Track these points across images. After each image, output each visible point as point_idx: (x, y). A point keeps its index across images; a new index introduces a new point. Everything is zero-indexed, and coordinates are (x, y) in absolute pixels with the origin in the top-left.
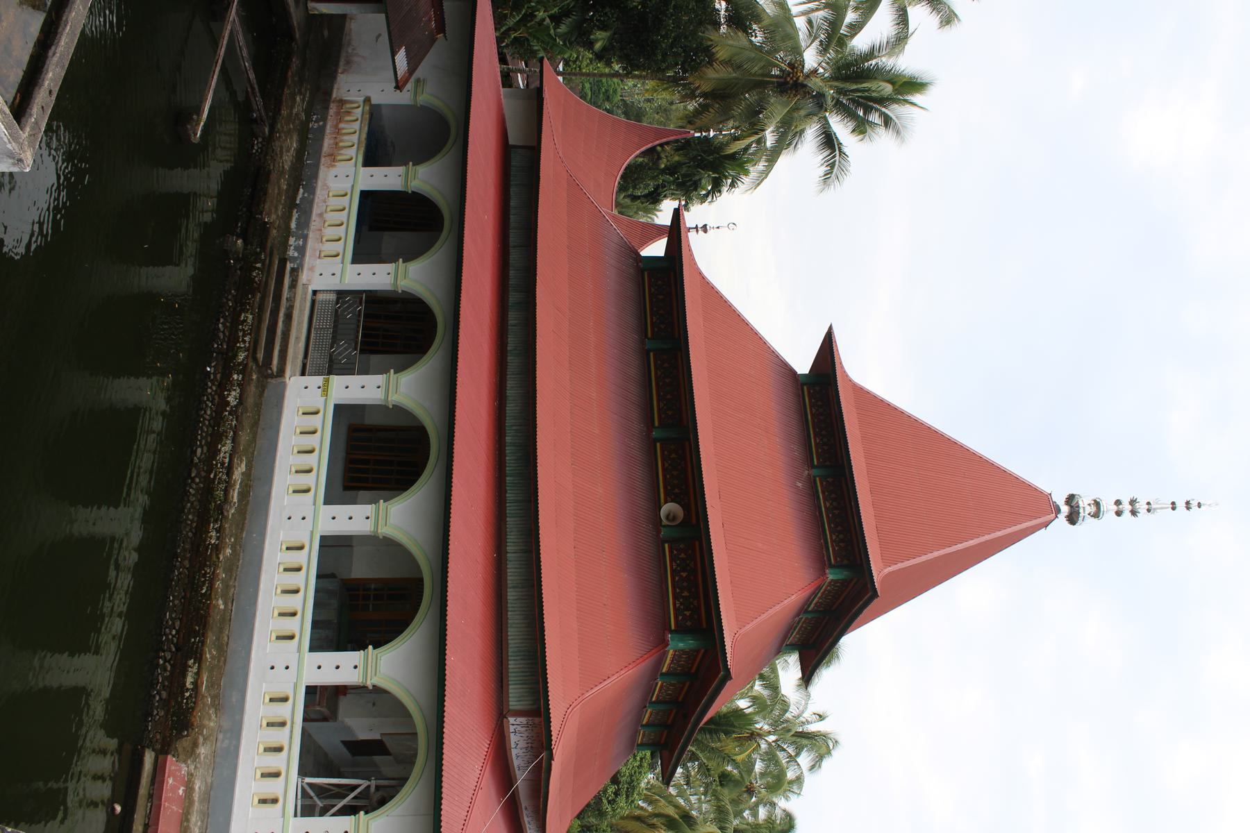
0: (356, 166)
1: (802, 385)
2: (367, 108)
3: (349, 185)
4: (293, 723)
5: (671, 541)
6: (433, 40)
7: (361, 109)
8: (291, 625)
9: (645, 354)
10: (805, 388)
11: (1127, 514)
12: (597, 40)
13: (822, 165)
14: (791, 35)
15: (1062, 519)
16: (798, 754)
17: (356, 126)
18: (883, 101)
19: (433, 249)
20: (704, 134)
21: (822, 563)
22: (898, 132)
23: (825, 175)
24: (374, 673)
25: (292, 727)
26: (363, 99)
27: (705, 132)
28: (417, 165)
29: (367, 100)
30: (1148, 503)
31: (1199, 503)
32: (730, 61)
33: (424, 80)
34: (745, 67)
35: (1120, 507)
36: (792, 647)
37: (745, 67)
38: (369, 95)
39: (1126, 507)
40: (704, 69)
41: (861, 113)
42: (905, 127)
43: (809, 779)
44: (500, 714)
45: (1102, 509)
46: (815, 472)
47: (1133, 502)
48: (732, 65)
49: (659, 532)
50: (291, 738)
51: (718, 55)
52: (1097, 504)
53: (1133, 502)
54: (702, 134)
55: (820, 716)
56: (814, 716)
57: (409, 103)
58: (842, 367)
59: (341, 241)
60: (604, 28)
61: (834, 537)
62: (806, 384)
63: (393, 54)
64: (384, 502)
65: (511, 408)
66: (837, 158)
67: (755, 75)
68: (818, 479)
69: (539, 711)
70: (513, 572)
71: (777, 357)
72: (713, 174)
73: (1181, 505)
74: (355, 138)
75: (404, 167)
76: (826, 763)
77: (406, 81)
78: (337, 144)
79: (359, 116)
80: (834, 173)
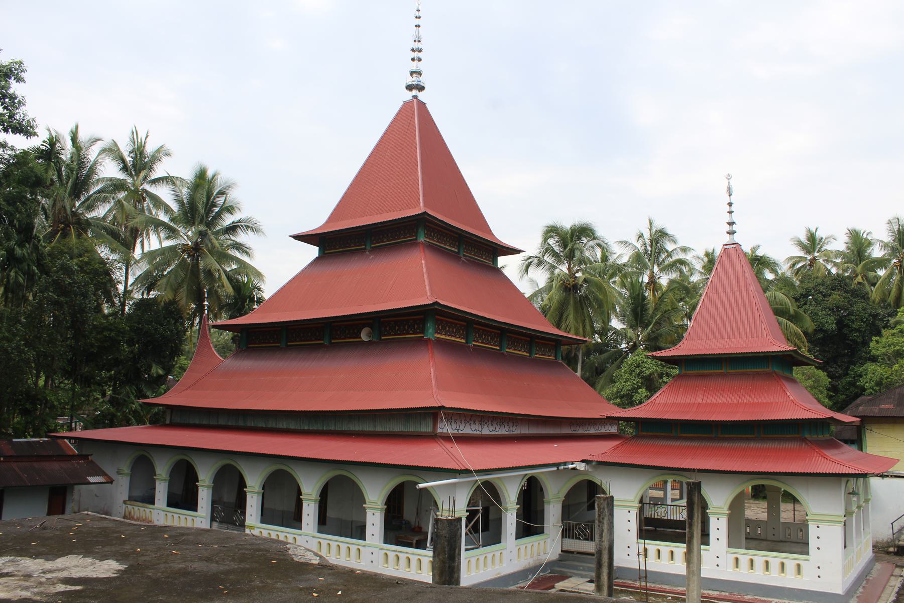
0: (154, 509)
1: (324, 254)
2: (128, 502)
3: (162, 512)
4: (396, 551)
5: (381, 335)
6: (92, 462)
7: (129, 506)
8: (354, 549)
9: (289, 348)
10: (326, 252)
11: (420, 55)
12: (157, 372)
13: (247, 233)
14: (172, 249)
15: (422, 96)
16: (667, 251)
17: (136, 508)
18: (209, 194)
19: (295, 477)
20: (206, 308)
21: (414, 244)
22: (229, 187)
23: (253, 231)
24: (376, 504)
25: (398, 551)
26: (124, 505)
27: (205, 307)
28: (155, 472)
29: (125, 502)
30: (415, 41)
31: (417, 10)
32: (175, 291)
33: (118, 469)
34: (180, 281)
35: (415, 58)
36: (495, 261)
37: (180, 281)
38: (122, 501)
39: (415, 55)
40: (180, 306)
41: (216, 209)
42: (226, 183)
43: (681, 243)
44: (433, 437)
45: (415, 70)
46: (368, 248)
47: (413, 50)
48: (177, 289)
49: (375, 342)
50: (403, 552)
51: (171, 298)
52: (412, 73)
53: (413, 50)
54: (206, 309)
55: (640, 237)
56: (639, 241)
57: (129, 478)
58: (315, 230)
59: (340, 545)
60: (150, 367)
61: (402, 237)
62: (324, 252)
63: (90, 483)
64: (302, 495)
65: (292, 426)
66: (243, 224)
67: (186, 275)
68: (372, 246)
69: (433, 413)
70: (368, 427)
71: (306, 268)
72: (246, 302)
73: (417, 22)
74: (142, 509)
75: (199, 487)
76: (670, 232)
77: (109, 477)
78: (143, 520)
79: (132, 507)
80: (252, 226)
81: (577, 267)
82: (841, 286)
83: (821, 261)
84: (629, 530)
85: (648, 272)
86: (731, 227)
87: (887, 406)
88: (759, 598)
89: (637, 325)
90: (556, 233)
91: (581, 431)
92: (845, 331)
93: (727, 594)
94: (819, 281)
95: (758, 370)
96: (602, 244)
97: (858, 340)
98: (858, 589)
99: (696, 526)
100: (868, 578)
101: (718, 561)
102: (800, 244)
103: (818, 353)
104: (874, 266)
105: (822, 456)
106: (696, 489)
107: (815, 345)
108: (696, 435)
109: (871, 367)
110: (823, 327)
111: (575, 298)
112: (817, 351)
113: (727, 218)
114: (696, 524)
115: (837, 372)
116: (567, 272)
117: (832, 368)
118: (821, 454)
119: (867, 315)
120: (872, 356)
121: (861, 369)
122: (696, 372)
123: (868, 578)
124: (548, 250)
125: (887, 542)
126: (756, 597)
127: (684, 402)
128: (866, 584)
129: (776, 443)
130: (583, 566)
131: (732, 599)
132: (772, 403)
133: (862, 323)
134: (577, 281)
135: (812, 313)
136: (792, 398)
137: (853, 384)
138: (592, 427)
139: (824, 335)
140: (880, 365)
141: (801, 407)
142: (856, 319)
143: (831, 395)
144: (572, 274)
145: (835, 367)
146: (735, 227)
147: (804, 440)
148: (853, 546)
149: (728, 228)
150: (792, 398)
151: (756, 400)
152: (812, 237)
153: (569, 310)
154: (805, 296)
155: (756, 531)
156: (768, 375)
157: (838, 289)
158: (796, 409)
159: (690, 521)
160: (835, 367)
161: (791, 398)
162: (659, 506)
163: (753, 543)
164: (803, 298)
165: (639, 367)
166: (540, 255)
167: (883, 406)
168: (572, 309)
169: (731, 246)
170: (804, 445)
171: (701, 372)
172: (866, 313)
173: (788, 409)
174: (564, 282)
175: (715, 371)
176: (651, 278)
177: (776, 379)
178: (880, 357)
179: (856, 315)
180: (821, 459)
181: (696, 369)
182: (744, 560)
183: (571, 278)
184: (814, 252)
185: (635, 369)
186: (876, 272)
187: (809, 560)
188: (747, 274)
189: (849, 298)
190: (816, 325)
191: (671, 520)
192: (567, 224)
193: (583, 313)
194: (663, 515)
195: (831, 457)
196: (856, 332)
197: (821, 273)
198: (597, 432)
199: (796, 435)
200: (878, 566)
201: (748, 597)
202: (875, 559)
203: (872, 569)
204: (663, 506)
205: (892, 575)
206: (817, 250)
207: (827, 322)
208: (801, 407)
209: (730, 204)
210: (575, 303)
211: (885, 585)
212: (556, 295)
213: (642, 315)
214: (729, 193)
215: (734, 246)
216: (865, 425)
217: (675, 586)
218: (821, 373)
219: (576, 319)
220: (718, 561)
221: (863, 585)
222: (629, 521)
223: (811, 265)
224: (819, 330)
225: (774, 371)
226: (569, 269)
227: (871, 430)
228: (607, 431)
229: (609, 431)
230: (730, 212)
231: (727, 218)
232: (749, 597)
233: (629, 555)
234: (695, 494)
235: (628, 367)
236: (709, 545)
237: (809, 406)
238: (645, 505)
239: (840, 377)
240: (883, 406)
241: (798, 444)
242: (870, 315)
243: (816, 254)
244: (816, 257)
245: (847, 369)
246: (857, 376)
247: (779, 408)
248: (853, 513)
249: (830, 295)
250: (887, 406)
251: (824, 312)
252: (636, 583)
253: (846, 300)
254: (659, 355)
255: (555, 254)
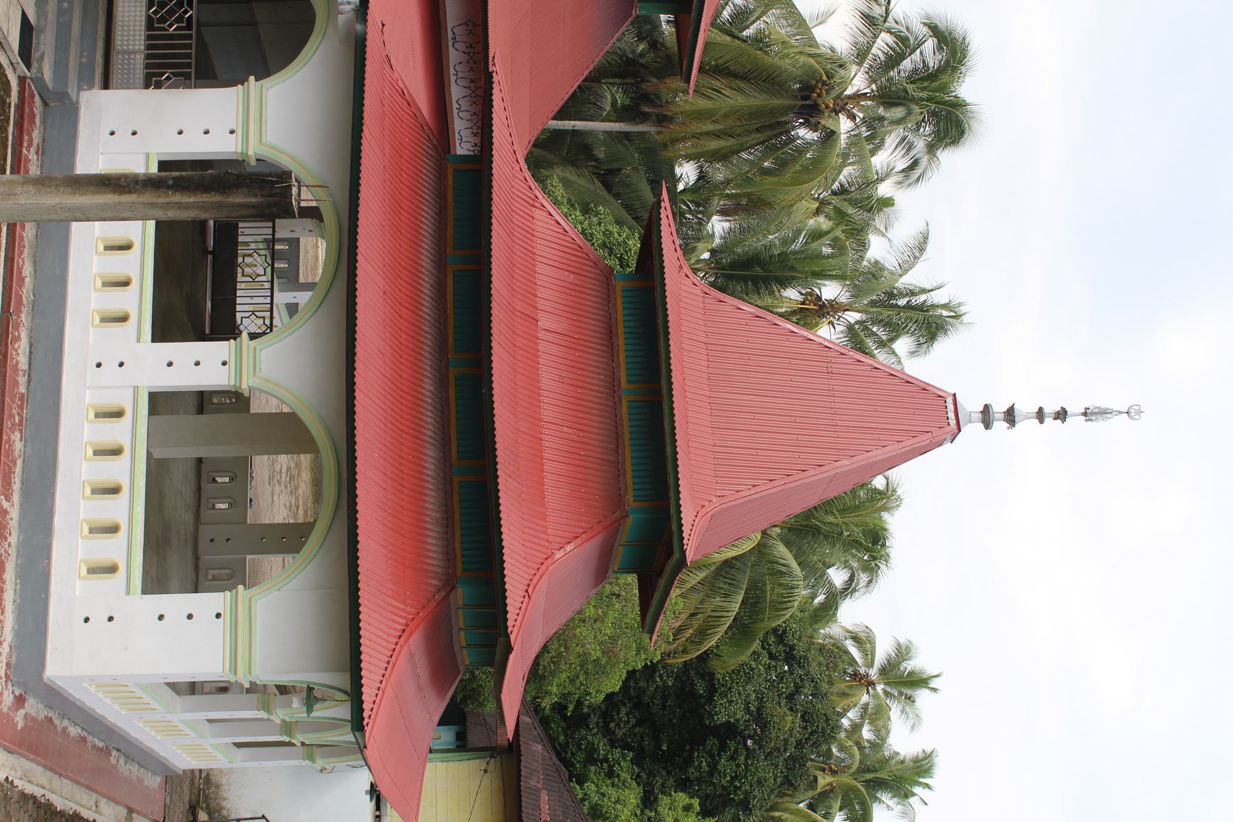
16: (892, 340)
81: (861, 115)
82: (811, 734)
83: (865, 698)
84: (180, 133)
85: (844, 298)
86: (1002, 416)
87: (545, 807)
88: (18, 469)
89: (719, 269)
90: (947, 62)
91: (454, 56)
92: (712, 742)
93: (22, 389)
94: (824, 686)
95: (629, 474)
96: (918, 172)
97: (691, 770)
98: (76, 724)
99: (155, 200)
100: (114, 753)
101: (110, 366)
102: (903, 652)
103: (660, 683)
104: (852, 810)
105: (407, 625)
106: (270, 199)
107: (677, 678)
108: (450, 312)
109: (632, 797)
110: (720, 694)
111: (785, 110)
112: (665, 682)
113: (1026, 407)
114: (162, 200)
115: (618, 725)
116: (849, 92)
117: (628, 714)
118: (412, 625)
119: (748, 788)
120: (656, 799)
121: (625, 775)
122: (620, 318)
123: (114, 753)
124: (904, 45)
125: (220, 809)
126: (19, 463)
127: (539, 282)
128: (94, 746)
129: (438, 515)
130: (70, 10)
131: (7, 399)
132: (543, 505)
133: (729, 778)
134: (826, 114)
135: (752, 669)
136: (558, 556)
137: (591, 759)
138: (467, 92)
139: (701, 696)
140: (636, 815)
141: (537, 577)
142: (738, 766)
143: (566, 708)
144: (841, 106)
145: (628, 722)
146: (1000, 426)
147: (449, 584)
148: (242, 762)
149: (999, 408)
150: (558, 556)
151: (549, 466)
152: (918, 681)
153: (757, 94)
154: (790, 657)
155: (221, 498)
156: (616, 501)
157: (805, 728)
158: (529, 564)
159: (171, 182)
160: (628, 722)
161: (559, 555)
162: (269, 261)
163: (180, 485)
164: (785, 651)
165: (621, 266)
166: (890, 23)
167: (544, 796)
168: (760, 103)
169: (951, 415)
170: (435, 582)
171: (621, 331)
172: (751, 786)
173: (527, 544)
174: (824, 83)
175: (623, 367)
176: (832, 306)
177: (606, 517)
178: (653, 813)
179: (746, 766)
180: (399, 624)
181: (627, 318)
182: (117, 433)
183: (835, 99)
184: (885, 684)
185: (615, 255)
186: (841, 810)
187: (128, 593)
188: (879, 452)
189: (786, 750)
190: (723, 678)
191: (235, 289)
192: (968, 89)
193: (749, 132)
194: (247, 270)
195: (405, 647)
196: (708, 766)
197: (837, 699)
198: (455, 106)
199: (460, 566)
200: (153, 782)
201: (17, 443)
202: (172, 779)
203: (140, 765)
204: (269, 270)
205: (130, 811)
206: (889, 689)
207: (731, 702)
208: (537, 577)
209: (1062, 415)
210: (773, 112)
211: (97, 792)
212: (790, 64)
213: (744, 279)
214: (1093, 414)
215: (953, 422)
216: (498, 757)
217: (34, 257)
218: (613, 684)
219: (734, 112)
220: (110, 366)
221: (90, 738)
222: (207, 132)
223: (856, 676)
224: (713, 685)
225: (627, 516)
226: (858, 96)
227: (486, 771)
228: (457, 136)
229: (458, 142)
230: (1040, 415)
231: (1026, 407)
232: (18, 446)
233: (112, 133)
234: (256, 196)
235: (620, 239)
236: (153, 341)
237: (539, 595)
238: (270, 224)
239: (607, 732)
240: (544, 796)
241: (438, 570)
242: (747, 793)
243: (880, 688)
244: (874, 689)
245: (626, 746)
246: (611, 767)
247: (524, 296)
248: (269, 711)
249: (791, 709)
250: (545, 807)
251: (753, 697)
252: (33, 150)
253: (780, 745)
254: (663, 216)
255: (893, 60)
